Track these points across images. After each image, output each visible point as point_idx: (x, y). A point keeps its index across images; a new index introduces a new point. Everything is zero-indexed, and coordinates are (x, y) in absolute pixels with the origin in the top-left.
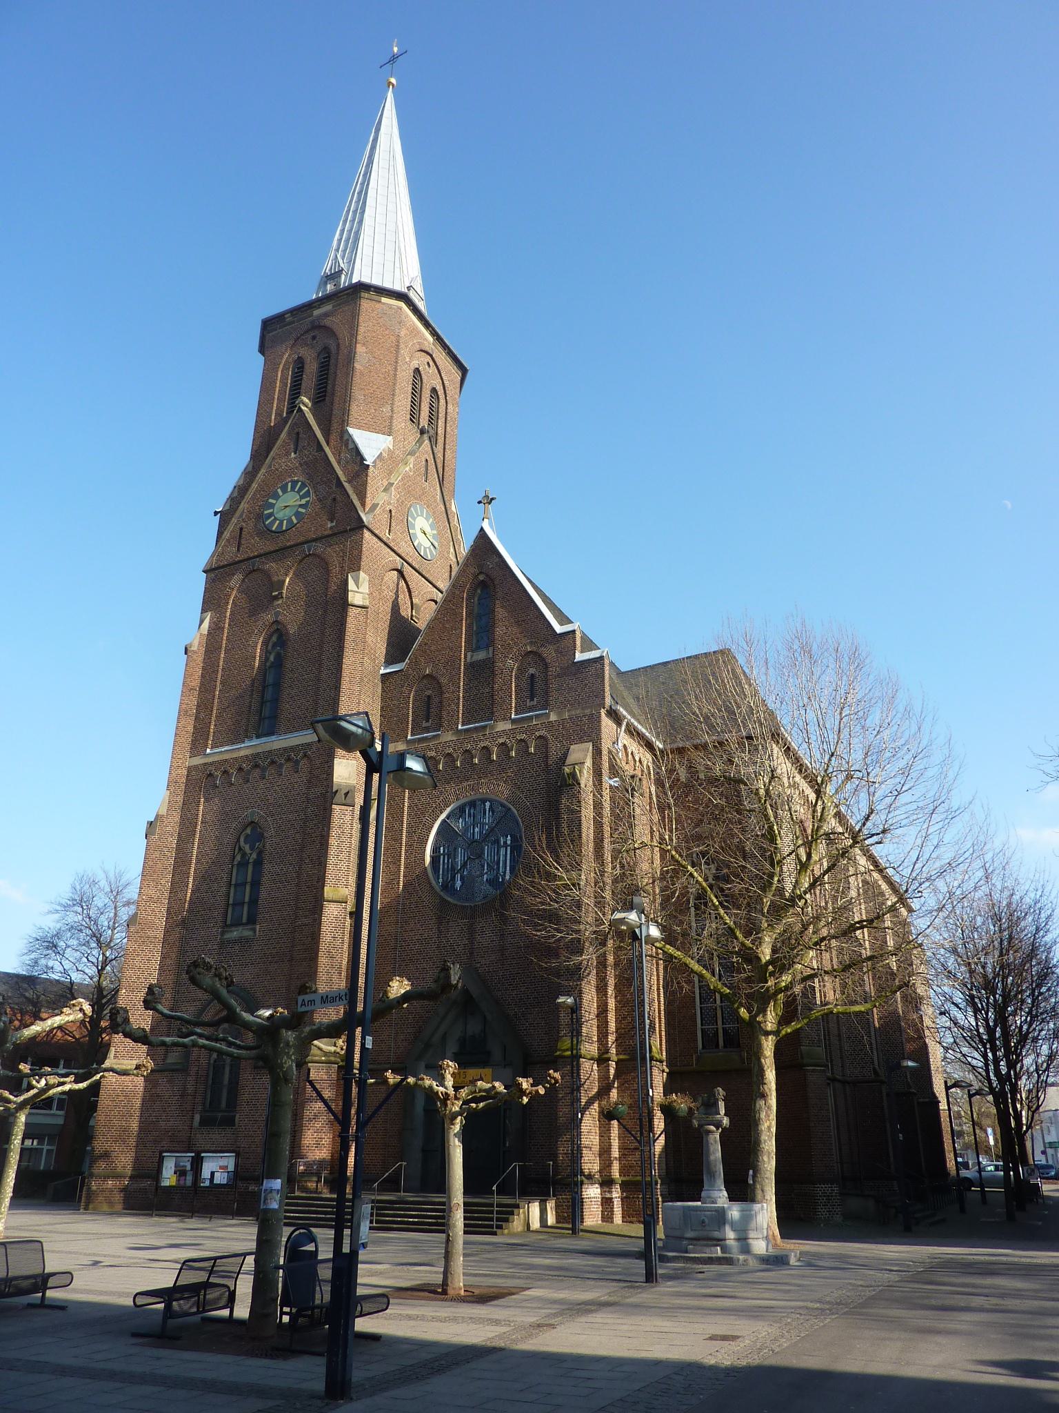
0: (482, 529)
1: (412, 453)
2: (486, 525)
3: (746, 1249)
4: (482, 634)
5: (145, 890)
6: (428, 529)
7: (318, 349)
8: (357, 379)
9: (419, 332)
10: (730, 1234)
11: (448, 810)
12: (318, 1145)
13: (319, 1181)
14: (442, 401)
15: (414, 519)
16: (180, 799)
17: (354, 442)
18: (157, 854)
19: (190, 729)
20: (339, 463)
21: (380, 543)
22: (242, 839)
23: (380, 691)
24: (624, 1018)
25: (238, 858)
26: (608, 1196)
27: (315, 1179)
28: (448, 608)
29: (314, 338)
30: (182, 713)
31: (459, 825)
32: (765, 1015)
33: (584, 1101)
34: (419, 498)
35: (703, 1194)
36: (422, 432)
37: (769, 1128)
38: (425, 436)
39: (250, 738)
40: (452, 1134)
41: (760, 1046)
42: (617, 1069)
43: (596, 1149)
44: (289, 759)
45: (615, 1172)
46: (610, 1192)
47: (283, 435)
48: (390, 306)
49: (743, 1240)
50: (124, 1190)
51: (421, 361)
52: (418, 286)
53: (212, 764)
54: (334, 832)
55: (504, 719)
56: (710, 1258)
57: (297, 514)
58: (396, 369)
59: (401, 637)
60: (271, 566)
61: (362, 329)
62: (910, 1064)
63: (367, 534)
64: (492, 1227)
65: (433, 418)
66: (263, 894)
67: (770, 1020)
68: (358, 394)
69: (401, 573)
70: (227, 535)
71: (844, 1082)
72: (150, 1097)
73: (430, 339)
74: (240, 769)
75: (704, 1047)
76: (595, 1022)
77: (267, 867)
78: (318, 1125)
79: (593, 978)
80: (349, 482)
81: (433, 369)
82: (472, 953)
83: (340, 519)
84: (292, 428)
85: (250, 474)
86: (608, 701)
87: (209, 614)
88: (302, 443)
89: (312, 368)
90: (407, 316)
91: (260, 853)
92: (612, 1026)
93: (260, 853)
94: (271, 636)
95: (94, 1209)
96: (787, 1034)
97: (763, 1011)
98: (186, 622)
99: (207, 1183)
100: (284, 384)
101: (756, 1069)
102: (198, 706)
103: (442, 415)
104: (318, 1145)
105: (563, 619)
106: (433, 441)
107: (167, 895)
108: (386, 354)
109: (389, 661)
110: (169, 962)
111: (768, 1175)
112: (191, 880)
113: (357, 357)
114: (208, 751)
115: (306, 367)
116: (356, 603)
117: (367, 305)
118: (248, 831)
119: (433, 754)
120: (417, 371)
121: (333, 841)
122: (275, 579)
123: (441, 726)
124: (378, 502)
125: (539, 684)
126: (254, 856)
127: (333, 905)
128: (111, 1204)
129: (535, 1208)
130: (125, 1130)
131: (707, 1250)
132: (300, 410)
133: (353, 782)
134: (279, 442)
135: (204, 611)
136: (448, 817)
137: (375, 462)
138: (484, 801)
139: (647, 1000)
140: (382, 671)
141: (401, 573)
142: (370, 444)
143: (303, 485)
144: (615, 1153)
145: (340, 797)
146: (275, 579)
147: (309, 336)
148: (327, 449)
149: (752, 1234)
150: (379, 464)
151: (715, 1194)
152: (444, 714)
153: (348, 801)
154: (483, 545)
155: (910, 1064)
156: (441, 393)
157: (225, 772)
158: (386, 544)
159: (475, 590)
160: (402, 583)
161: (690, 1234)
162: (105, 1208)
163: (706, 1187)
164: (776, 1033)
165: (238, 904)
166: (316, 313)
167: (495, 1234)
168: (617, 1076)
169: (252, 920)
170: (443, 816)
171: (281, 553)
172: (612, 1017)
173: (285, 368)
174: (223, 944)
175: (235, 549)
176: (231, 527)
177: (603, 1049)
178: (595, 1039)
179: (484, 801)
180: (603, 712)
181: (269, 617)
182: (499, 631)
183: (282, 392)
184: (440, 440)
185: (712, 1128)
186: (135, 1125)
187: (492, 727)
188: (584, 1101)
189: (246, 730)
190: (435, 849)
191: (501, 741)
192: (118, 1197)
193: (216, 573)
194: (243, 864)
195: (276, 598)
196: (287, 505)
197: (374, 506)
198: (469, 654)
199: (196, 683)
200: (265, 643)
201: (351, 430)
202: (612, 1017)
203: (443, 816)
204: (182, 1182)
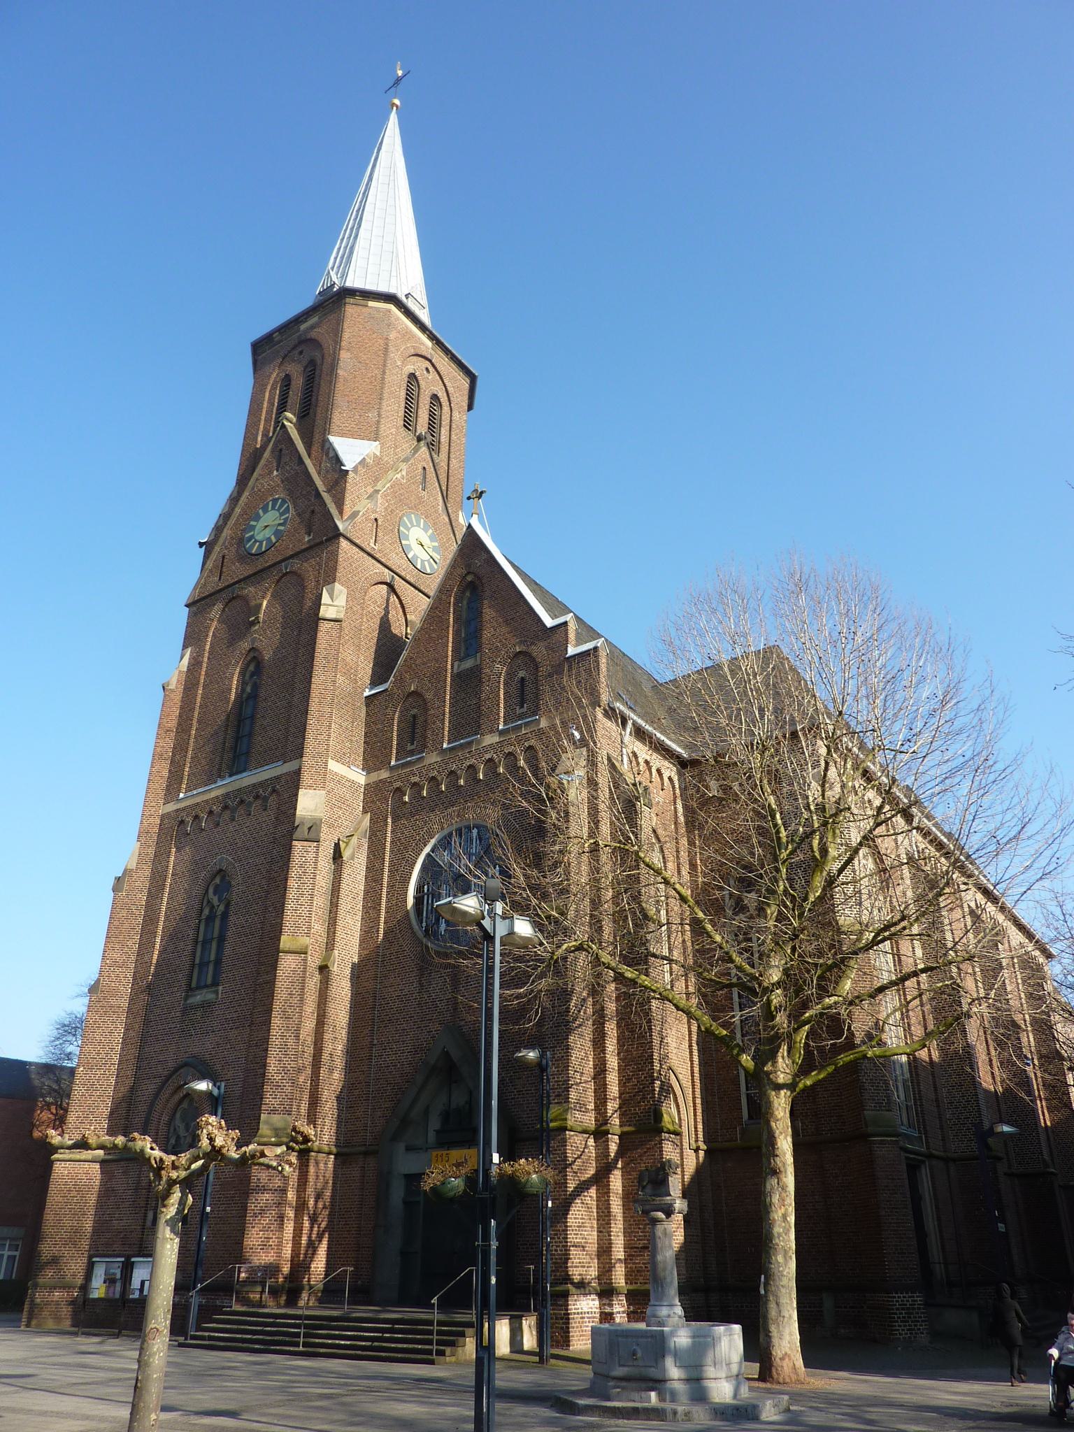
0: (470, 526)
1: (406, 460)
2: (475, 522)
3: (699, 1394)
4: (470, 642)
5: (110, 954)
6: (426, 541)
7: (305, 363)
8: (340, 386)
9: (414, 336)
10: (674, 1372)
11: (433, 842)
12: (264, 1246)
13: (263, 1292)
14: (446, 409)
15: (408, 529)
16: (151, 851)
17: (334, 450)
18: (124, 913)
19: (166, 773)
20: (319, 473)
21: (362, 554)
22: (211, 891)
23: (363, 714)
24: (629, 1080)
25: (206, 912)
26: (608, 1310)
27: (259, 1289)
28: (435, 615)
29: (301, 353)
30: (157, 756)
31: (444, 858)
32: (775, 1063)
33: (571, 1186)
34: (415, 507)
35: (649, 1311)
36: (419, 439)
37: (785, 1217)
38: (422, 443)
39: (223, 778)
40: (162, 1221)
41: (769, 1104)
42: (620, 1146)
43: (592, 1248)
44: (257, 797)
45: (619, 1277)
46: (611, 1305)
47: (267, 454)
48: (377, 309)
49: (695, 1380)
50: (73, 1303)
51: (418, 366)
52: (420, 294)
53: (183, 809)
54: (294, 873)
55: (491, 732)
56: (636, 1410)
57: (277, 533)
58: (384, 372)
59: (388, 650)
60: (250, 590)
61: (346, 335)
62: (1006, 1129)
63: (342, 539)
64: (430, 1352)
65: (431, 426)
66: (227, 951)
67: (783, 1068)
68: (340, 400)
69: (391, 587)
70: (210, 564)
71: (946, 1160)
72: (106, 1192)
73: (429, 343)
74: (211, 812)
75: (750, 1117)
76: (592, 1085)
77: (232, 918)
78: (265, 1222)
79: (588, 1031)
80: (328, 491)
81: (433, 375)
82: (455, 1009)
83: (319, 535)
84: (275, 445)
85: (234, 500)
86: (605, 698)
87: (189, 650)
88: (285, 459)
89: (298, 382)
90: (398, 319)
91: (227, 906)
92: (614, 1089)
93: (227, 906)
94: (248, 665)
95: (38, 1326)
96: (806, 1088)
97: (772, 1056)
98: (173, 664)
99: (136, 1295)
100: (271, 403)
101: (765, 1137)
102: (174, 748)
103: (445, 422)
104: (264, 1246)
105: (555, 606)
106: (433, 447)
107: (133, 958)
108: (378, 363)
109: (374, 684)
110: (132, 1033)
111: (784, 1281)
112: (158, 940)
113: (341, 364)
114: (182, 795)
115: (293, 383)
116: (328, 616)
117: (351, 310)
118: (217, 880)
119: (416, 779)
120: (412, 376)
121: (292, 883)
122: (253, 603)
123: (424, 746)
124: (358, 511)
125: (529, 688)
126: (222, 908)
127: (290, 957)
128: (58, 1319)
129: (503, 1329)
130: (77, 1231)
131: (635, 1395)
132: (284, 426)
133: (319, 814)
134: (263, 462)
135: (185, 647)
136: (433, 850)
137: (355, 469)
138: (469, 828)
139: (656, 1056)
140: (367, 693)
141: (391, 587)
142: (350, 450)
143: (284, 501)
144: (619, 1252)
145: (302, 832)
146: (253, 603)
147: (296, 352)
148: (308, 462)
149: (710, 1371)
150: (362, 470)
151: (664, 1311)
152: (429, 733)
153: (312, 835)
154: (472, 545)
155: (1006, 1129)
156: (444, 399)
157: (196, 817)
158: (369, 554)
159: (463, 592)
160: (393, 598)
161: (620, 1371)
162: (51, 1324)
163: (652, 1302)
164: (791, 1086)
165: (203, 965)
166: (303, 327)
167: (432, 1362)
168: (621, 1152)
169: (215, 983)
170: (427, 849)
171: (256, 577)
172: (613, 1079)
173: (274, 388)
174: (185, 1011)
175: (216, 579)
176: (214, 556)
177: (602, 1120)
178: (591, 1106)
179: (469, 828)
180: (599, 713)
181: (245, 645)
182: (487, 634)
183: (269, 412)
184: (444, 448)
185: (661, 1215)
186: (88, 1225)
187: (479, 742)
188: (571, 1186)
189: (220, 770)
190: (419, 889)
191: (488, 756)
192: (66, 1311)
193: (198, 605)
194: (210, 919)
195: (253, 624)
196: (267, 526)
197: (355, 514)
198: (456, 664)
199: (173, 723)
200: (242, 673)
201: (331, 438)
202: (613, 1079)
203: (427, 849)
204: (111, 1295)
